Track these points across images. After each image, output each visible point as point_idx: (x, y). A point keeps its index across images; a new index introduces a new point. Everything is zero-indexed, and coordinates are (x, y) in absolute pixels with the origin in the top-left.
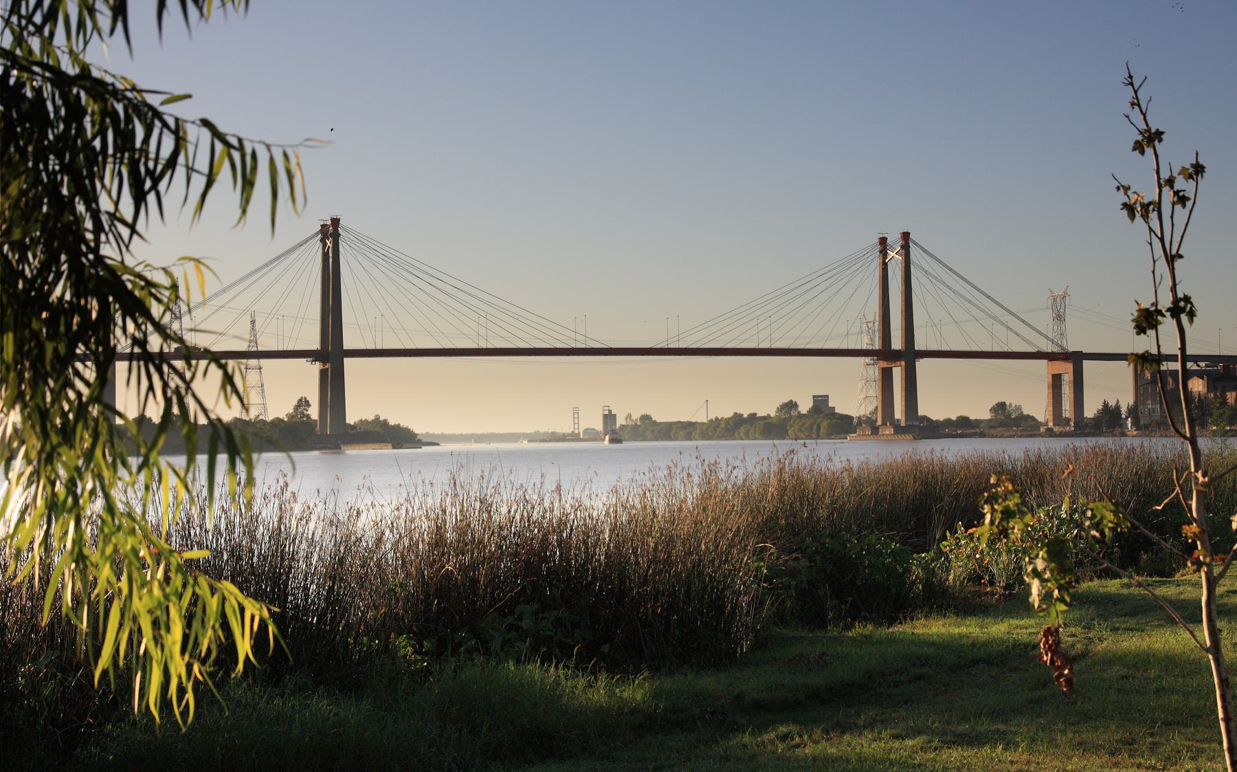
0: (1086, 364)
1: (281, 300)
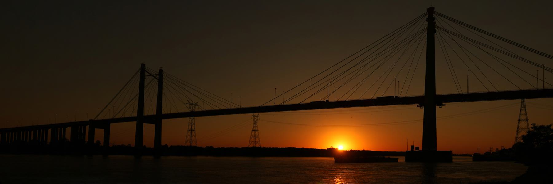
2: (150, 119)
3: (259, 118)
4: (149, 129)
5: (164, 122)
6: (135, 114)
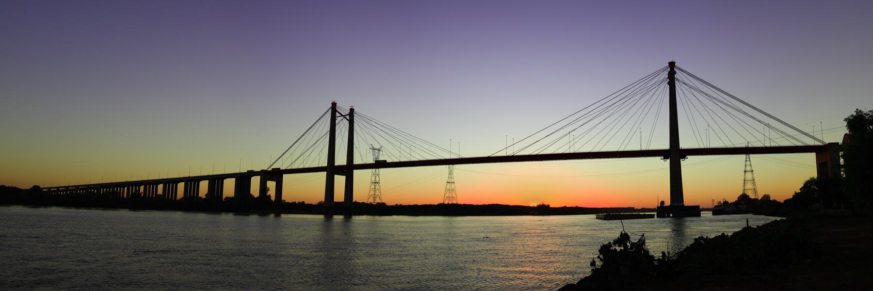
0: (286, 177)
1: (659, 109)
2: (341, 170)
3: (381, 152)
4: (340, 181)
5: (356, 173)
6: (325, 164)
